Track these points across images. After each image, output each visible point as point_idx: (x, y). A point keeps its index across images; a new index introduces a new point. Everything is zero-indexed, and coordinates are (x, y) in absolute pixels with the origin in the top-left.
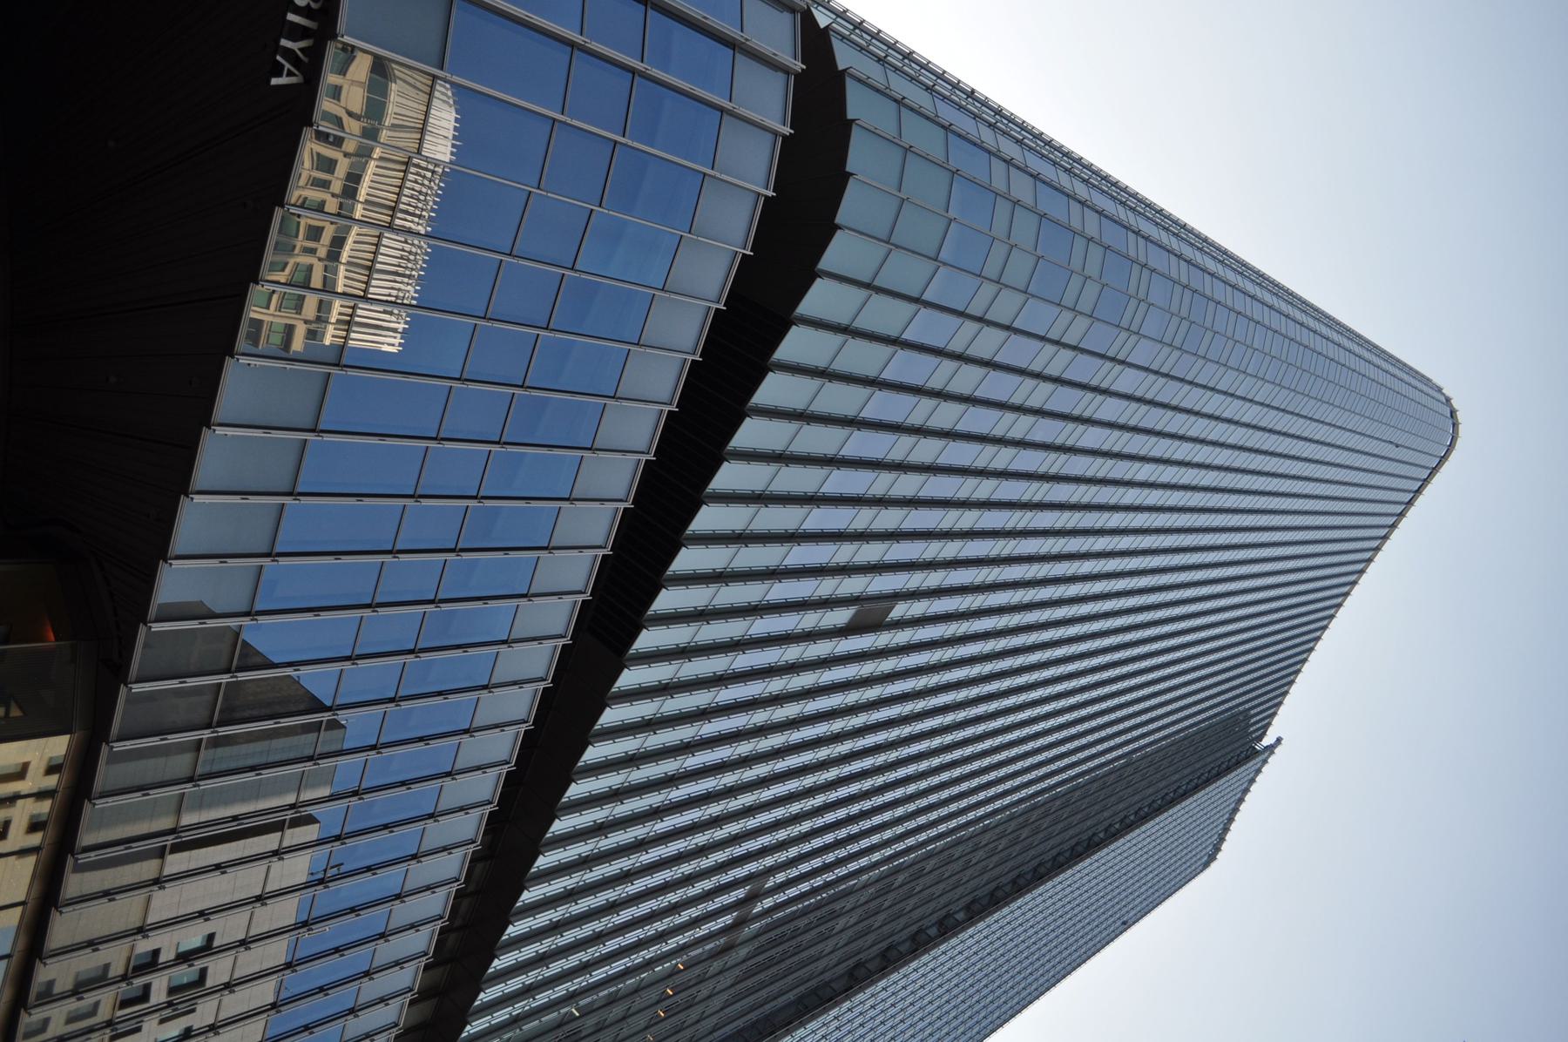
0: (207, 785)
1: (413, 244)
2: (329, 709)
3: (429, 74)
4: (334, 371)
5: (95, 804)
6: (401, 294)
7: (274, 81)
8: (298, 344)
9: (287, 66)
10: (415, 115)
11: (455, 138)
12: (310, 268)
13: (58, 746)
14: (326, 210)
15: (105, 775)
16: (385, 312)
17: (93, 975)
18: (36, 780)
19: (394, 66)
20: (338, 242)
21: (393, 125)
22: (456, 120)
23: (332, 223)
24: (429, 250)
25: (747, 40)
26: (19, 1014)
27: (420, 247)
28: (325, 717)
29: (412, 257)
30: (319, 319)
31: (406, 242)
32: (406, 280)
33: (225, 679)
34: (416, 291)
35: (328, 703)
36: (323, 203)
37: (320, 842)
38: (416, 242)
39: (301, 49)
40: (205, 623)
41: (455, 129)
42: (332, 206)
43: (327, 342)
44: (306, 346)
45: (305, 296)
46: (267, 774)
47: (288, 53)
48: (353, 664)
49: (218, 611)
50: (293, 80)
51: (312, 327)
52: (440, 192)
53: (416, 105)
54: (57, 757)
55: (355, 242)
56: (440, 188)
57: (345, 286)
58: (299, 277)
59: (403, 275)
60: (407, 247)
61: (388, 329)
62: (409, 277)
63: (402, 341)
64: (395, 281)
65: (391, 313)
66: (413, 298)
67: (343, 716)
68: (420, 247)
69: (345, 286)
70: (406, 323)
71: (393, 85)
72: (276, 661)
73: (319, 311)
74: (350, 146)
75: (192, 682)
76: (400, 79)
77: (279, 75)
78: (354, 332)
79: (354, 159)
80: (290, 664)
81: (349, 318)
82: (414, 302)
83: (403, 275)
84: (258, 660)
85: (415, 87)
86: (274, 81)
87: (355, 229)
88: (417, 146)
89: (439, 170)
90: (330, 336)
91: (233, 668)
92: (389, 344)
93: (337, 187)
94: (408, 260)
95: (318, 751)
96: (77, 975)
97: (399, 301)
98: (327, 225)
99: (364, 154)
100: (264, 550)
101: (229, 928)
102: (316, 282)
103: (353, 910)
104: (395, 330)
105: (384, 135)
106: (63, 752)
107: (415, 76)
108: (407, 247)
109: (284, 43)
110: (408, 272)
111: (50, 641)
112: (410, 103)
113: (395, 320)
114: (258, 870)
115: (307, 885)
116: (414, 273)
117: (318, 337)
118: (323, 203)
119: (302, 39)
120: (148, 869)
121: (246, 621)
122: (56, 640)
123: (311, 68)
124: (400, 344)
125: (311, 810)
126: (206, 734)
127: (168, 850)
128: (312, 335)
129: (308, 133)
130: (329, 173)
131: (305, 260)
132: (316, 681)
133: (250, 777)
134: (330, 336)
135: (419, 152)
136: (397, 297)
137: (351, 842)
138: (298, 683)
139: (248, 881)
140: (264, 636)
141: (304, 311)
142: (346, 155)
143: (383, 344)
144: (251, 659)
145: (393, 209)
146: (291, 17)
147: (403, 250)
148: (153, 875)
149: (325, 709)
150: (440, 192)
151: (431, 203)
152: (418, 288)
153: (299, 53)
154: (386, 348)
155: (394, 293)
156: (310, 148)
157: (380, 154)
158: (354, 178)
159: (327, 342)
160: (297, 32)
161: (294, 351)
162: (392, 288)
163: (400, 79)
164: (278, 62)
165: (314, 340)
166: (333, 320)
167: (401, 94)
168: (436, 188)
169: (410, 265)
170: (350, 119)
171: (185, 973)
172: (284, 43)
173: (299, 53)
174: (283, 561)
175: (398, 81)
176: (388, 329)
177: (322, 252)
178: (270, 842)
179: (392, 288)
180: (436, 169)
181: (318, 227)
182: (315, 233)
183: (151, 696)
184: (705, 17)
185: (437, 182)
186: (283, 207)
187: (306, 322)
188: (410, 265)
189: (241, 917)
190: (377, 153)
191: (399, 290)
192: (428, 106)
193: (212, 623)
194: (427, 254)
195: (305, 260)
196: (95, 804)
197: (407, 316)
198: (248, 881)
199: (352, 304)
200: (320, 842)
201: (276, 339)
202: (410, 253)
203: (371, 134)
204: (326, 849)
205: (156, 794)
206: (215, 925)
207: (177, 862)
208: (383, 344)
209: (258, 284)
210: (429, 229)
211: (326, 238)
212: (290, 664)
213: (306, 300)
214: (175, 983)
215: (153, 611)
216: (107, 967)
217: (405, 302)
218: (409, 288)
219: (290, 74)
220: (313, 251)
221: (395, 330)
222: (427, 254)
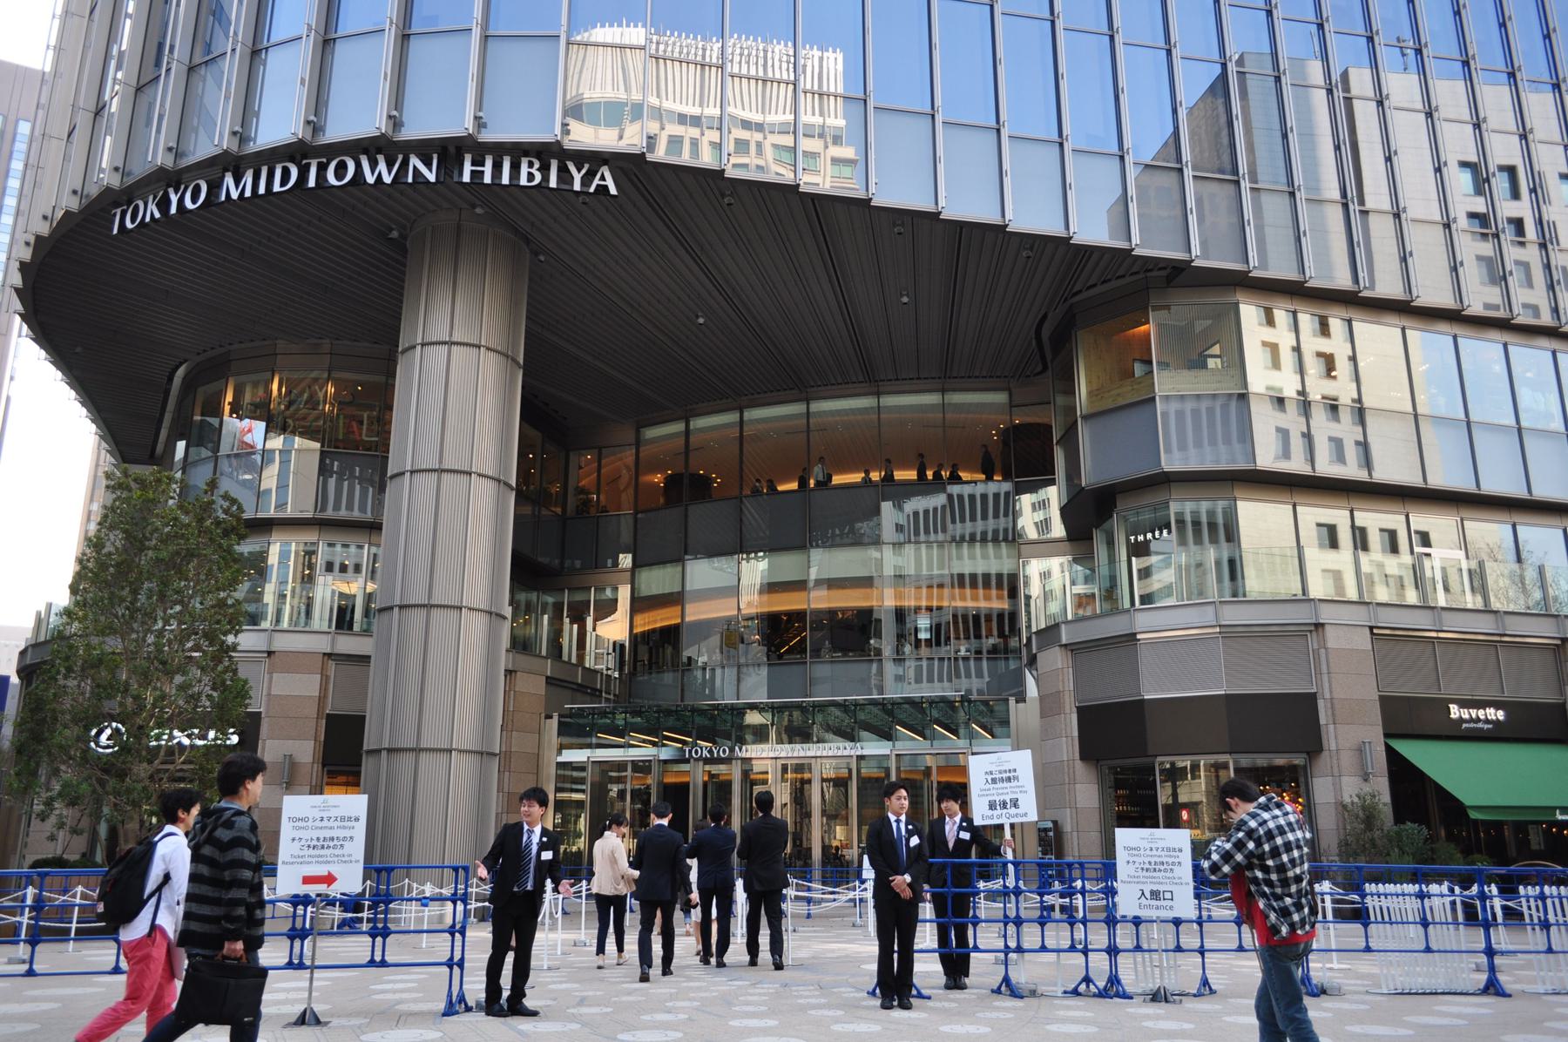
0: (1299, 179)
1: (733, 54)
2: (1224, 66)
3: (567, 49)
4: (871, 104)
5: (1311, 277)
6: (785, 58)
7: (613, 191)
8: (848, 152)
9: (596, 181)
10: (609, 58)
11: (620, 25)
12: (775, 146)
13: (1249, 313)
14: (680, 589)
15: (1281, 269)
16: (804, 72)
17: (1484, 271)
18: (1282, 336)
19: (568, 97)
20: (746, 125)
21: (626, 91)
22: (603, 26)
23: (730, 132)
24: (736, 36)
25: (391, 22)
26: (1517, 325)
27: (734, 45)
28: (1232, 68)
29: (746, 52)
30: (821, 136)
31: (732, 61)
32: (769, 55)
33: (1188, 173)
34: (779, 43)
35: (1217, 70)
36: (712, 143)
37: (1374, 65)
38: (730, 50)
39: (579, 171)
40: (1132, 198)
41: (611, 25)
42: (714, 136)
43: (841, 122)
44: (848, 144)
45: (804, 151)
46: (1291, 121)
47: (587, 180)
48: (1175, 47)
49: (1119, 192)
50: (608, 175)
51: (829, 140)
52: (676, 34)
53: (600, 58)
54: (1258, 316)
55: (744, 109)
56: (672, 34)
57: (784, 113)
58: (787, 157)
59: (765, 58)
60: (737, 58)
61: (821, 67)
62: (765, 51)
63: (830, 49)
64: (773, 66)
65: (805, 66)
66: (786, 45)
67: (1233, 51)
68: (734, 45)
69: (784, 113)
70: (812, 48)
71: (585, 96)
72: (1171, 129)
73: (814, 137)
74: (653, 127)
75: (1191, 202)
76: (578, 89)
77: (606, 187)
78: (828, 89)
79: (665, 122)
80: (1175, 111)
81: (816, 96)
82: (790, 44)
83: (765, 58)
84: (1172, 140)
85: (581, 72)
86: (613, 191)
87: (730, 109)
88: (638, 51)
89: (655, 38)
90: (837, 121)
91: (1178, 166)
92: (836, 64)
93: (694, 132)
94: (749, 55)
95: (1271, 72)
96: (1482, 283)
97: (792, 60)
98: (732, 137)
99: (658, 114)
100: (1056, 149)
101: (1458, 143)
102: (788, 140)
103: (1454, 269)
104: (821, 59)
105: (636, 96)
106: (1253, 308)
107: (573, 63)
108: (737, 58)
109: (577, 187)
110: (762, 54)
111: (1151, 328)
112: (600, 63)
113: (810, 61)
114: (1397, 121)
115: (1422, 71)
116: (761, 48)
117: (838, 133)
118: (712, 143)
119: (568, 171)
120: (1382, 229)
121: (1129, 159)
122: (1148, 323)
123: (593, 160)
124: (834, 52)
125: (1336, 76)
126: (1245, 185)
127: (1362, 208)
128: (837, 140)
129: (650, 157)
130: (682, 142)
131: (769, 152)
132: (1194, 83)
133: (1293, 139)
134: (837, 121)
135: (643, 48)
136: (788, 62)
137: (1377, 24)
138: (1191, 108)
139: (1409, 130)
140: (1146, 141)
141: (816, 151)
142: (663, 129)
143: (836, 70)
144: (1170, 162)
145: (703, 66)
146: (553, 183)
147: (740, 63)
148: (1389, 221)
149: (1224, 75)
150: (676, 34)
151: (689, 41)
152: (775, 41)
153: (583, 171)
154: (840, 67)
155: (784, 65)
156: (660, 154)
157: (655, 97)
158: (682, 119)
159: (841, 122)
160: (563, 172)
161: (856, 155)
162: (780, 68)
163: (578, 89)
164: (596, 190)
165: (842, 137)
166: (820, 120)
167: (592, 87)
168: (673, 39)
169: (754, 53)
170: (625, 137)
171: (1500, 184)
172: (577, 187)
173: (583, 171)
174: (1066, 130)
175: (580, 92)
176: (821, 67)
177: (758, 136)
178: (1365, 113)
179: (780, 68)
180: (654, 41)
181: (736, 143)
182: (742, 146)
183: (1204, 244)
184: (385, 79)
185: (666, 38)
186: (724, 170)
187: (826, 147)
188: (754, 53)
189: (1447, 132)
190: (654, 101)
191: (780, 61)
192: (597, 45)
193: (1132, 191)
194: (739, 38)
195: (769, 152)
196: (1311, 277)
197: (805, 49)
198: (1409, 130)
199: (802, 95)
200: (1374, 65)
201: (847, 171)
202: (741, 55)
203: (637, 111)
204: (1381, 52)
205: (1304, 225)
206: (1452, 156)
207: (1376, 196)
208: (836, 70)
209: (799, 185)
210: (714, 39)
211: (744, 134)
212: (1175, 111)
213: (805, 149)
214: (1508, 195)
215: (1121, 244)
216: (1479, 258)
217: (791, 53)
218: (777, 50)
219: (603, 178)
220: (759, 145)
221: (821, 59)
222: (739, 38)
